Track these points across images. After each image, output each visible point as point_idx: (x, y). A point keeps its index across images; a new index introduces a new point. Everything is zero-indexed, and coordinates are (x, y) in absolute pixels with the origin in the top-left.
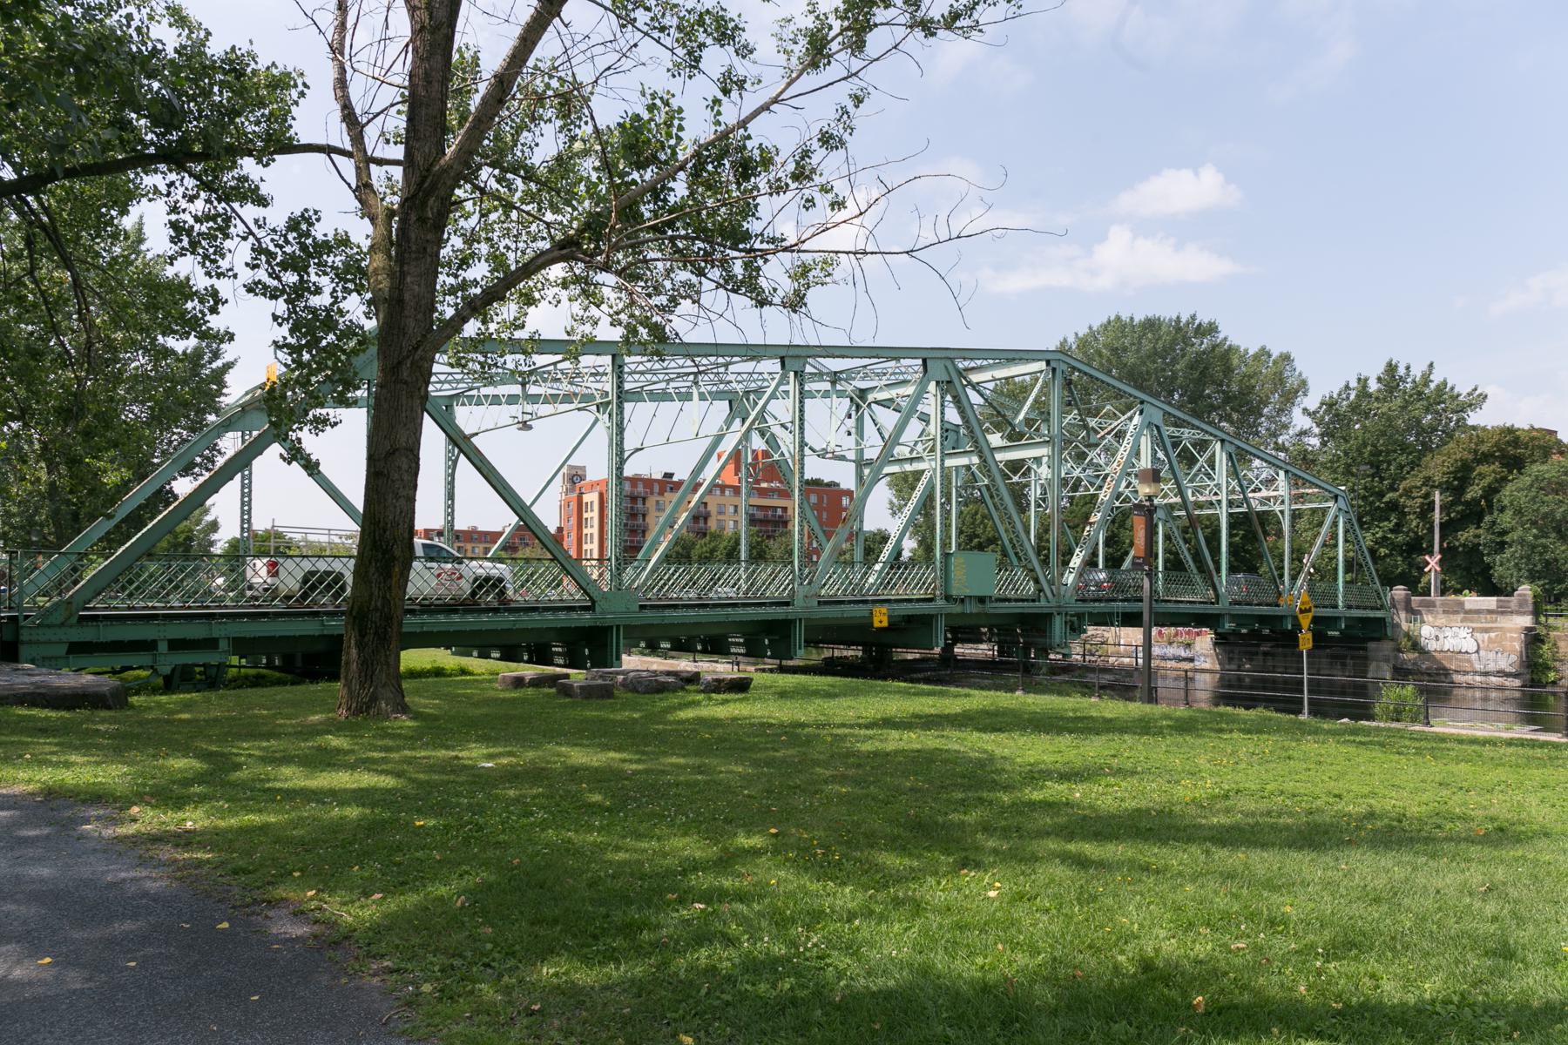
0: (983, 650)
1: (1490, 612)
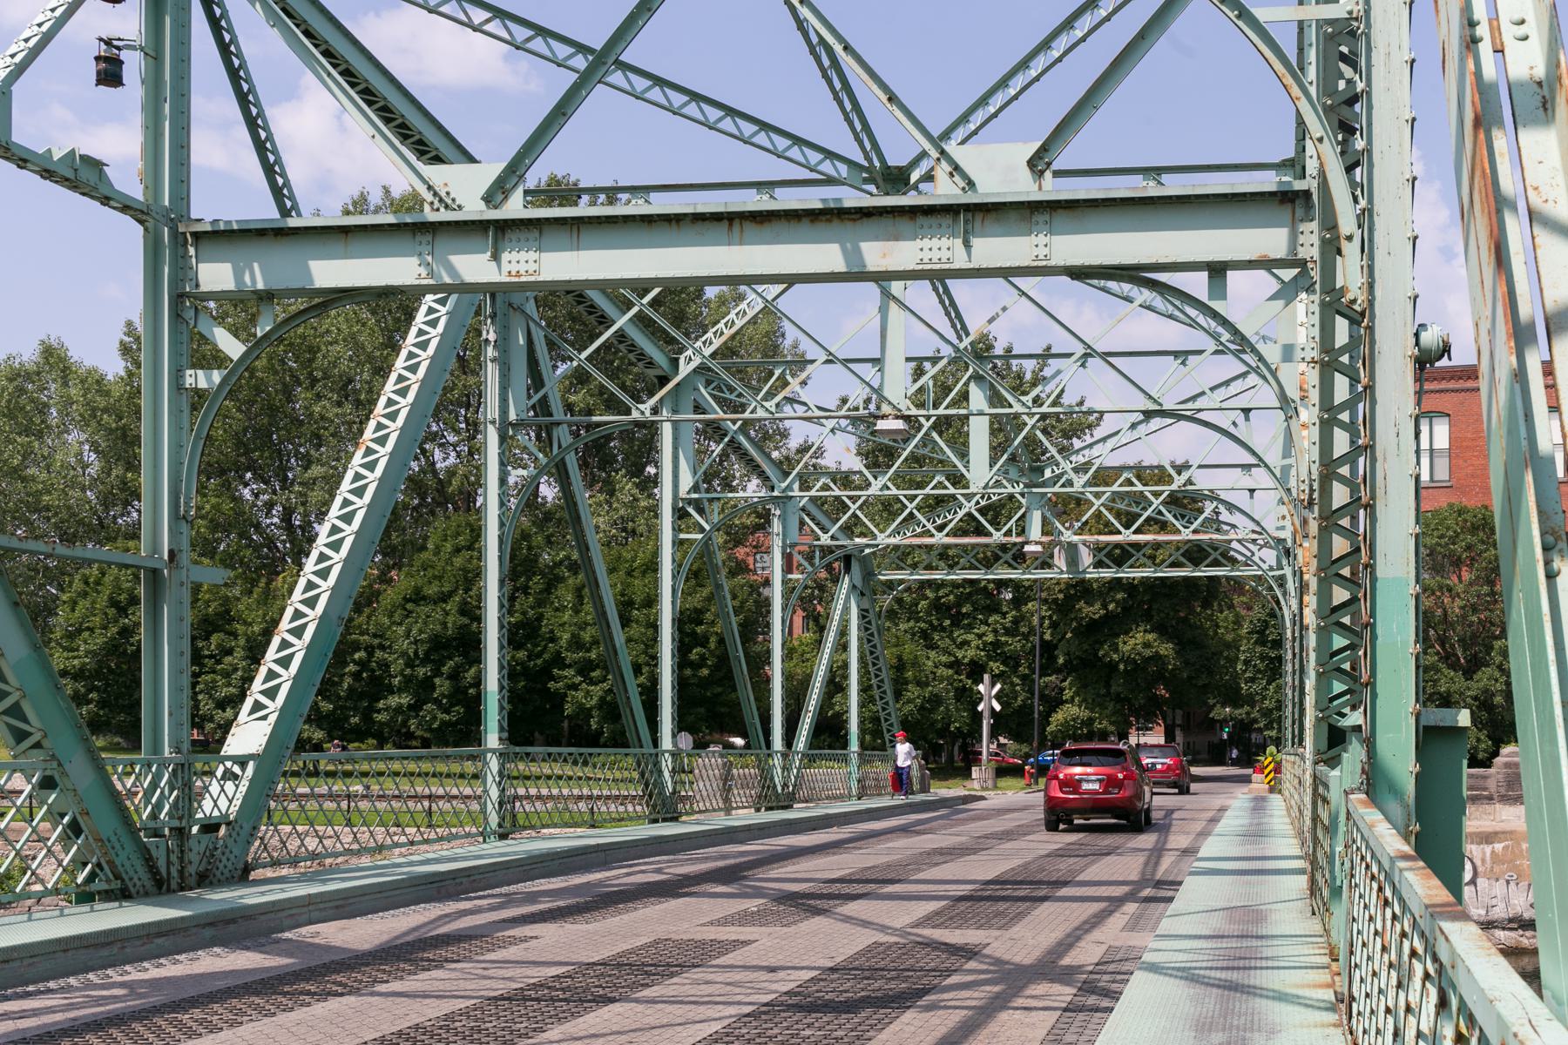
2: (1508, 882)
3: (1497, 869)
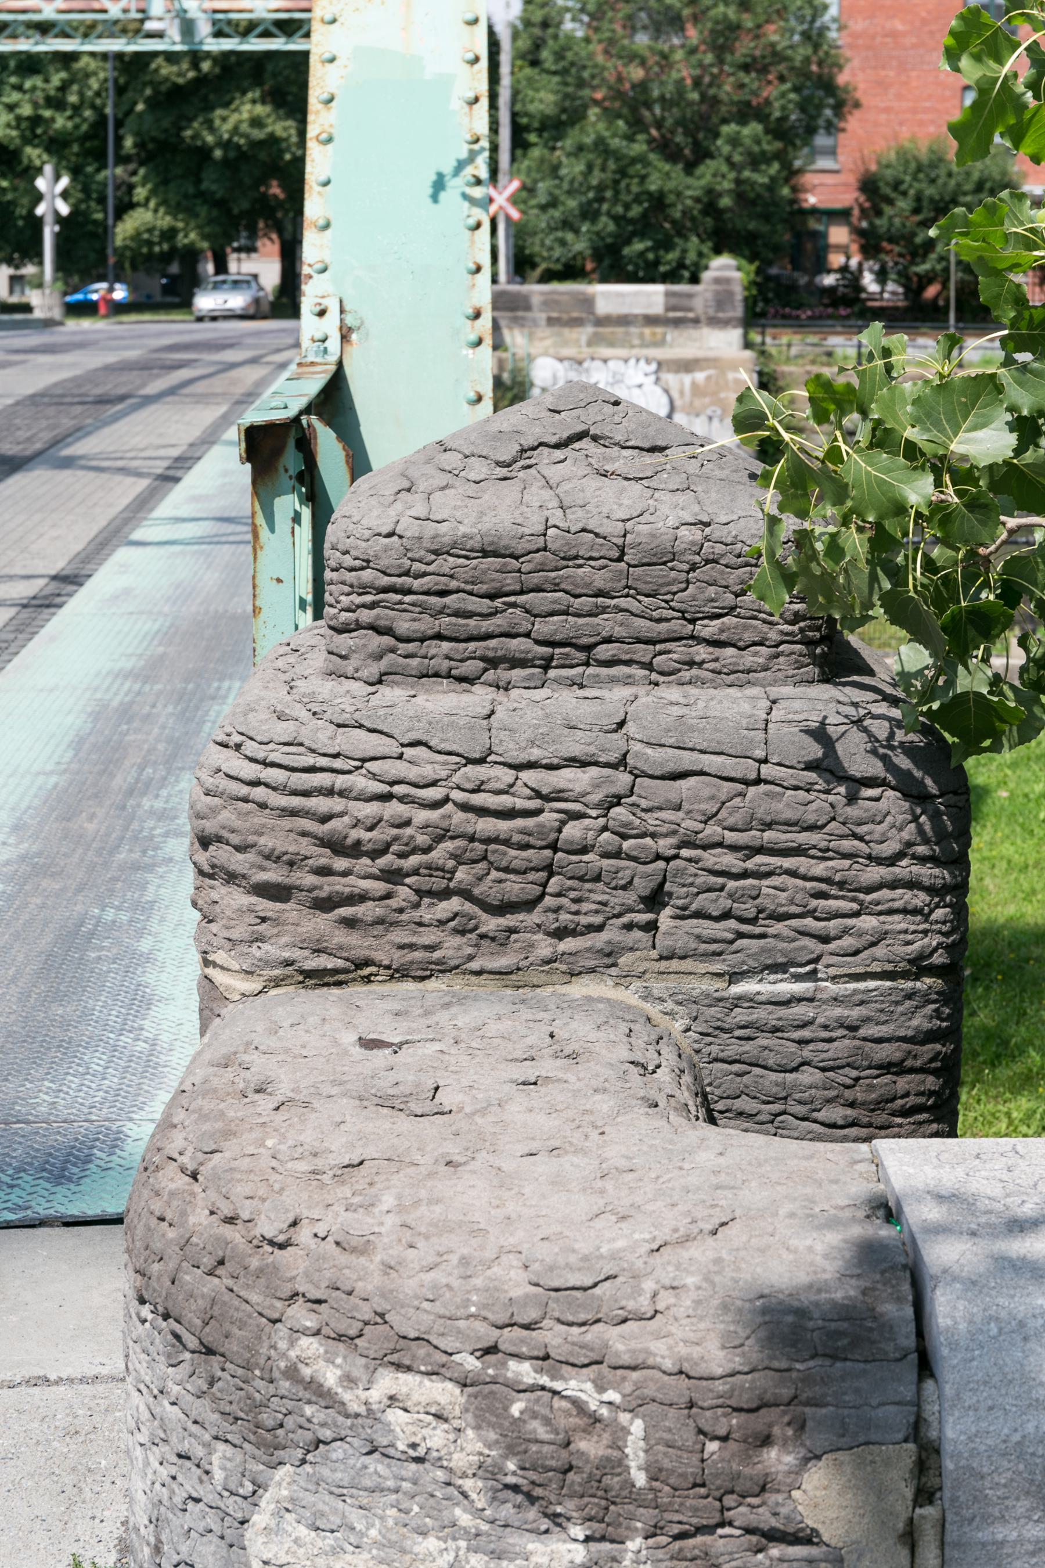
0: (940, 683)
1: (651, 320)
2: (710, 418)
3: (697, 403)
